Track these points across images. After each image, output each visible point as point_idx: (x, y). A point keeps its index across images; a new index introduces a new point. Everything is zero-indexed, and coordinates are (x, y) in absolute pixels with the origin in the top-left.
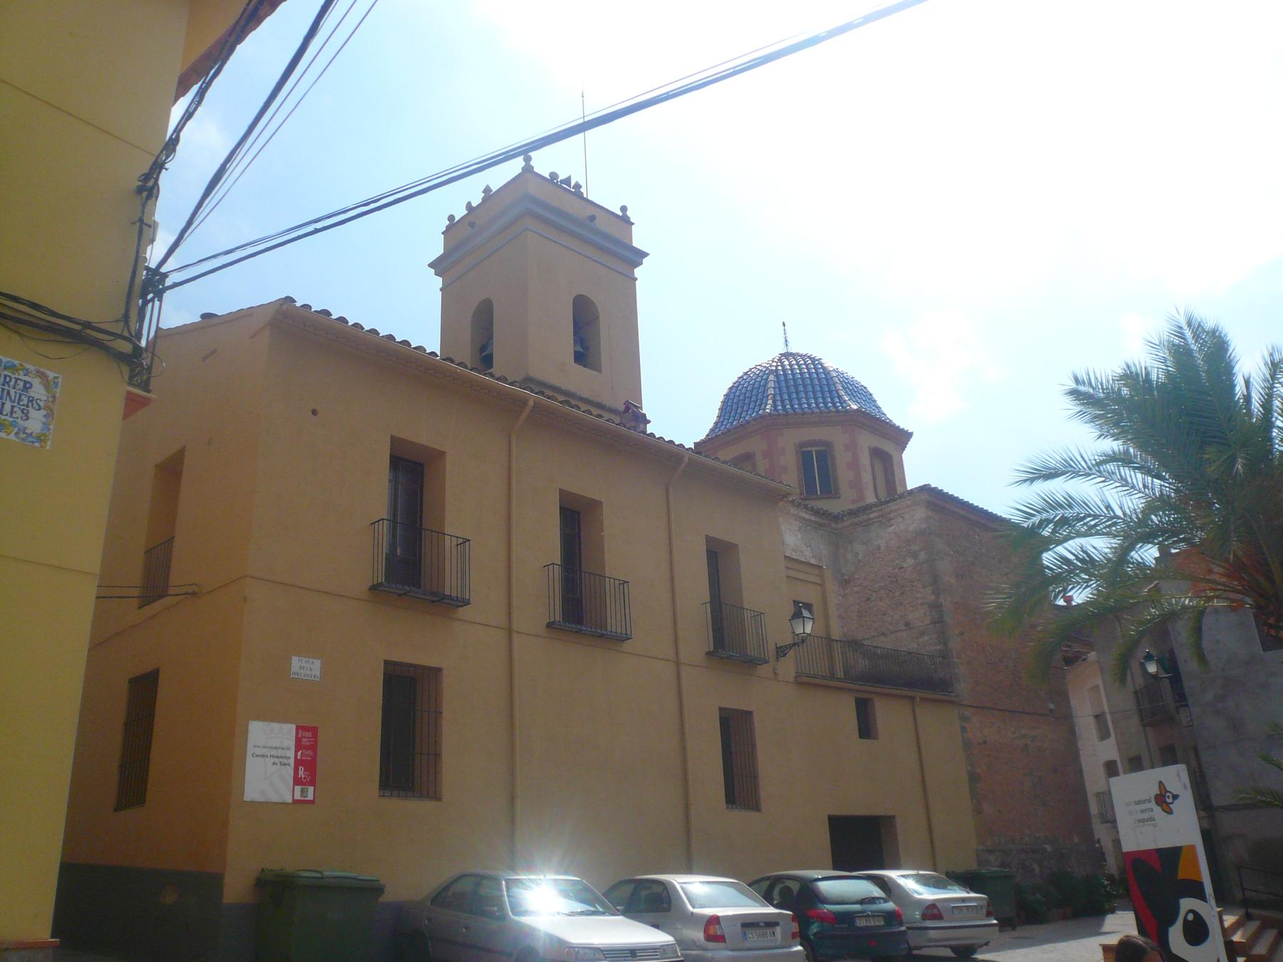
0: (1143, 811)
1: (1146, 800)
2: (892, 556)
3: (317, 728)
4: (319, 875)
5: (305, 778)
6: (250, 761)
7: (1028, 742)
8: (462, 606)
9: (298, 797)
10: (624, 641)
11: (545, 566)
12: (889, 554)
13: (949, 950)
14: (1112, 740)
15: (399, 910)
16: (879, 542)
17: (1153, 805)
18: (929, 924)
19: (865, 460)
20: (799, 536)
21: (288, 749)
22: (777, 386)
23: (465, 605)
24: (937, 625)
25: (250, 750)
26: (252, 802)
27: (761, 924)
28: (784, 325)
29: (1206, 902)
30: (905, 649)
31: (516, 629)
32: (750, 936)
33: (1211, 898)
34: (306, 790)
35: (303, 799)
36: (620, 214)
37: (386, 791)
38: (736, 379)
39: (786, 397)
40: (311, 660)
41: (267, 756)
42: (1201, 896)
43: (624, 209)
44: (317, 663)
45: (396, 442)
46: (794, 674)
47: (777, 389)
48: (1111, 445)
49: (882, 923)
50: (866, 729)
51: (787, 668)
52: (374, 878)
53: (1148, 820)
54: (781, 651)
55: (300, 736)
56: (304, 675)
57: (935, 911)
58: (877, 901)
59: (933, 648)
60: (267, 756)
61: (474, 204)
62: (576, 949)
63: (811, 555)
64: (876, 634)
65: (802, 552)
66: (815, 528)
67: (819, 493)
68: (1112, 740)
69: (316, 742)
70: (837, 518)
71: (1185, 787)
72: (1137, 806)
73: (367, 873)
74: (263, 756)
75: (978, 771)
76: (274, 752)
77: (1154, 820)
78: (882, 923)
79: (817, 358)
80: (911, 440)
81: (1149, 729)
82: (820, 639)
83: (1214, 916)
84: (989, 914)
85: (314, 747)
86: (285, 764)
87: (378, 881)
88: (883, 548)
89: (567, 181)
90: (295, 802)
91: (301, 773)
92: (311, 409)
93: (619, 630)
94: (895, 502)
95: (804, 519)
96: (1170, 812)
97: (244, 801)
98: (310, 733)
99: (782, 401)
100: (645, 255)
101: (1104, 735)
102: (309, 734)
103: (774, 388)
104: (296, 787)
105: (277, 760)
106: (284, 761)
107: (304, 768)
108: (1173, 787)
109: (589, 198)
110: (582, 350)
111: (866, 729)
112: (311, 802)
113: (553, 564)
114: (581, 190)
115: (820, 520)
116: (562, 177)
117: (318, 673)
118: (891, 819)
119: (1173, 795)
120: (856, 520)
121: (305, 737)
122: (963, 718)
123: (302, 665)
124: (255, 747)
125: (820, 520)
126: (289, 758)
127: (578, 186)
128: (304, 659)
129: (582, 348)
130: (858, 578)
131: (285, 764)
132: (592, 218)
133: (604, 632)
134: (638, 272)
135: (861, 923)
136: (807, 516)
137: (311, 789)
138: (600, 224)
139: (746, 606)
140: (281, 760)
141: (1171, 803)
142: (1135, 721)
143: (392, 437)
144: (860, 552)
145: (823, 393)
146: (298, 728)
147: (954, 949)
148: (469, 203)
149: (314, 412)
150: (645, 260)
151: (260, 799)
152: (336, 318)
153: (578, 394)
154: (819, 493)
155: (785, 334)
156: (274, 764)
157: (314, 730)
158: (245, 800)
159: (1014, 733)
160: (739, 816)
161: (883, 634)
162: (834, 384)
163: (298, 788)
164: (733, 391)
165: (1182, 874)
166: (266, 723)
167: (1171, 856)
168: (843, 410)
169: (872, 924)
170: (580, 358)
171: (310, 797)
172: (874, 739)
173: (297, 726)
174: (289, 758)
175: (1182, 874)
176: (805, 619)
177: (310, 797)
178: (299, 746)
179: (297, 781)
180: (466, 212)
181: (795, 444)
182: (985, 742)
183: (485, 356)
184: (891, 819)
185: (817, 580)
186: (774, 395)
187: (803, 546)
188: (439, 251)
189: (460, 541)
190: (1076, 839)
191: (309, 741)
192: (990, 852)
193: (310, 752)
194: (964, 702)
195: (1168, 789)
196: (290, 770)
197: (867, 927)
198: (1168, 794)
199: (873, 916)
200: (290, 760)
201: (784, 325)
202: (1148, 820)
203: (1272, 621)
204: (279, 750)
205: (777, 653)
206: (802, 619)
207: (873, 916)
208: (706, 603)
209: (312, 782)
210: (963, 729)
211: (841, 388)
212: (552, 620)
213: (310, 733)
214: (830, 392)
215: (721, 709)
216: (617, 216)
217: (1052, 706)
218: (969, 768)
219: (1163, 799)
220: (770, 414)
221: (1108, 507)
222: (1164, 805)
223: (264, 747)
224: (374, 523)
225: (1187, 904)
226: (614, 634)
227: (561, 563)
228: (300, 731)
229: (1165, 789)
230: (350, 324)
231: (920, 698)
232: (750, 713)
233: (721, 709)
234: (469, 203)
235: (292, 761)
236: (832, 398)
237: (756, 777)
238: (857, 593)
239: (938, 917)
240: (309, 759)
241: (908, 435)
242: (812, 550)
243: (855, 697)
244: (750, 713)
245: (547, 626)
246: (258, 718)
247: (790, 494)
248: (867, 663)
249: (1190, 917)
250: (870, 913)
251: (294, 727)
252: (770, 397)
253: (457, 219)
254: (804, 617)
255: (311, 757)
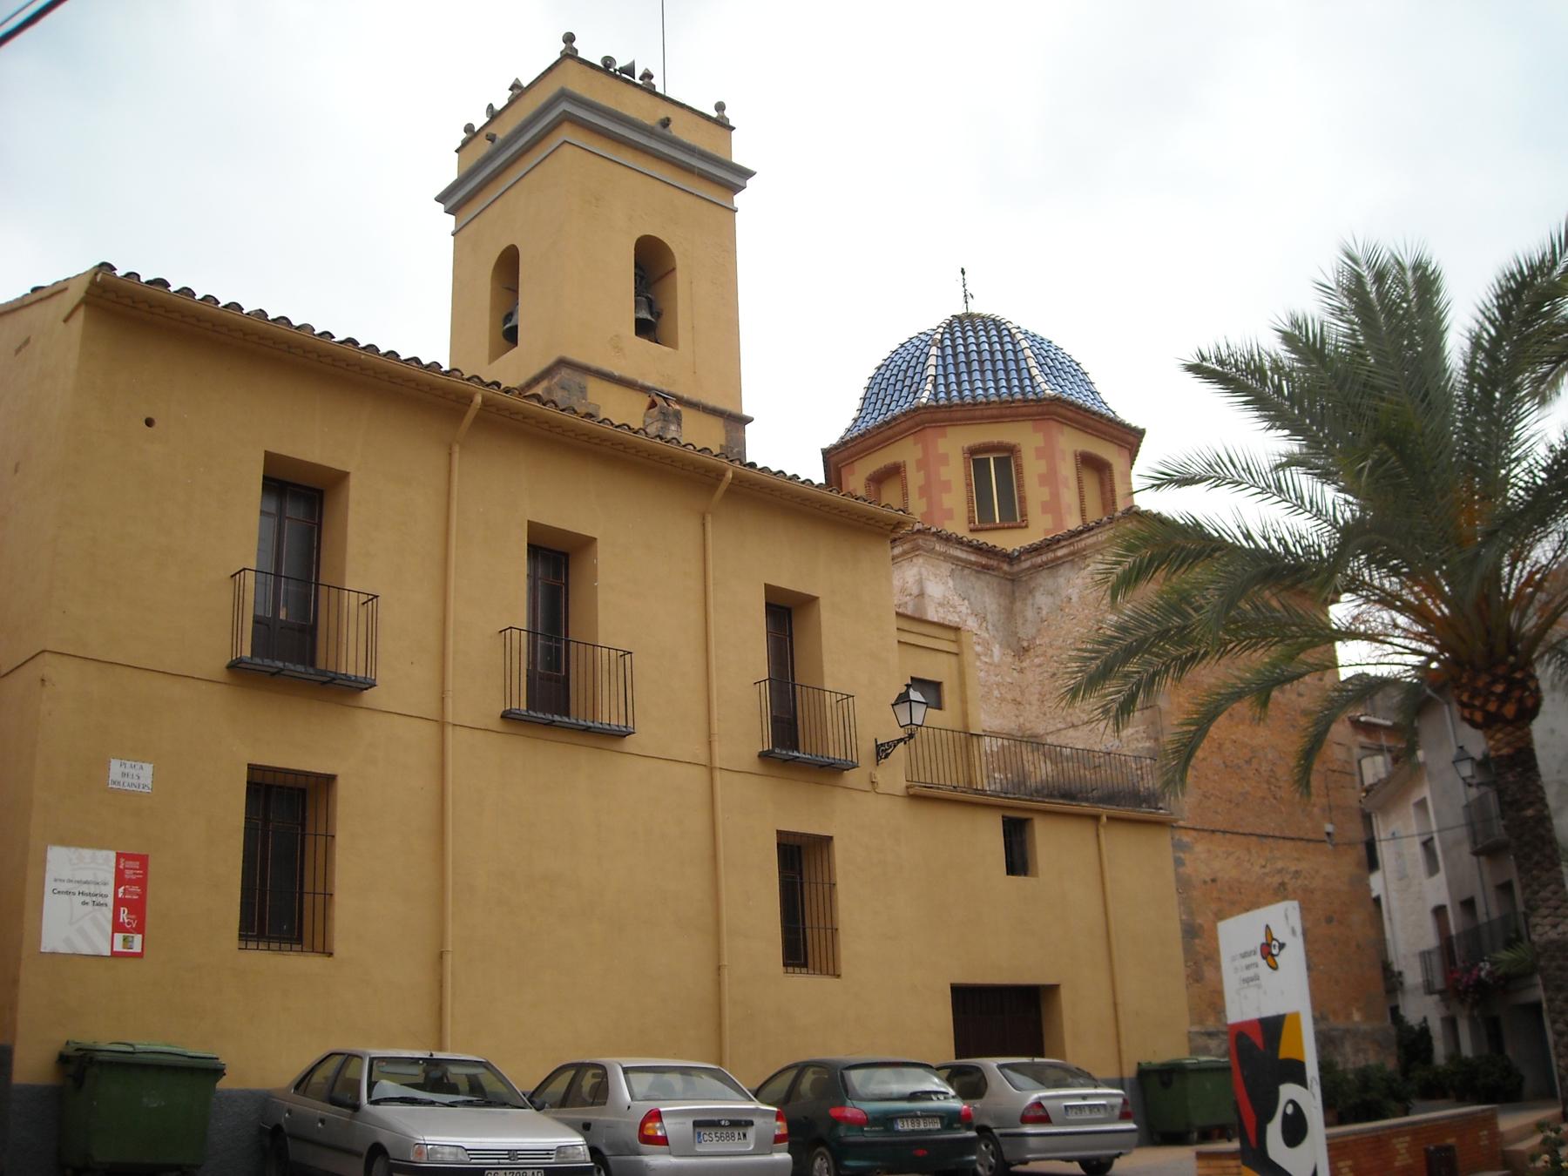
0: (1248, 967)
1: (1251, 952)
2: (1086, 611)
3: (147, 856)
4: (131, 1049)
5: (129, 923)
6: (50, 902)
7: (1286, 880)
8: (366, 689)
9: (118, 947)
10: (625, 736)
11: (501, 632)
12: (1083, 609)
13: (1076, 1164)
14: (1441, 877)
15: (264, 1101)
16: (1070, 591)
17: (1258, 958)
18: (1029, 1129)
19: (1067, 469)
20: (951, 583)
21: (105, 884)
22: (940, 362)
23: (371, 687)
24: (1145, 711)
25: (49, 885)
26: (53, 954)
27: (723, 1123)
28: (963, 272)
29: (1306, 1087)
30: (1103, 748)
31: (450, 721)
32: (706, 1137)
33: (1314, 1083)
34: (130, 939)
35: (126, 950)
36: (714, 114)
37: (260, 943)
38: (888, 354)
39: (952, 378)
40: (138, 764)
41: (74, 894)
42: (1301, 1080)
43: (720, 107)
44: (148, 769)
45: (271, 459)
46: (904, 784)
47: (940, 368)
48: (1294, 447)
49: (938, 1126)
50: (1018, 861)
51: (894, 774)
52: (215, 1056)
53: (1252, 979)
54: (882, 751)
55: (121, 867)
56: (129, 785)
57: (1041, 1113)
58: (934, 1097)
59: (1140, 746)
60: (74, 894)
61: (498, 107)
62: (429, 1147)
63: (969, 611)
64: (1063, 726)
65: (954, 607)
66: (977, 572)
67: (998, 521)
68: (1441, 877)
69: (145, 874)
70: (1009, 558)
71: (1294, 932)
72: (1243, 960)
73: (192, 1046)
74: (68, 893)
75: (1199, 921)
76: (85, 888)
77: (1258, 979)
78: (938, 1126)
79: (1003, 321)
80: (1144, 440)
81: (1483, 859)
82: (950, 733)
83: (1316, 1108)
84: (1125, 1116)
85: (142, 882)
86: (99, 904)
87: (217, 1059)
88: (1075, 599)
89: (630, 70)
90: (115, 955)
91: (124, 916)
92: (144, 419)
93: (614, 722)
94: (1092, 533)
95: (958, 559)
96: (1274, 967)
97: (41, 953)
98: (138, 863)
99: (947, 386)
100: (747, 174)
101: (1433, 868)
102: (136, 864)
103: (936, 367)
104: (116, 934)
105: (88, 899)
106: (101, 900)
107: (128, 910)
108: (1280, 934)
109: (667, 95)
110: (649, 317)
111: (1018, 861)
112: (139, 955)
113: (511, 628)
114: (653, 81)
115: (984, 561)
116: (621, 63)
117: (149, 782)
118: (951, 984)
119: (1279, 943)
120: (1039, 560)
121: (127, 869)
122: (1178, 846)
123: (126, 771)
124: (56, 880)
125: (984, 561)
126: (106, 896)
127: (647, 76)
128: (128, 763)
129: (652, 314)
130: (1040, 645)
131: (99, 904)
132: (666, 123)
133: (591, 724)
134: (739, 200)
135: (903, 1126)
136: (963, 555)
137: (138, 938)
138: (681, 129)
139: (828, 685)
140: (94, 899)
141: (1277, 955)
142: (1466, 848)
143: (267, 454)
144: (1043, 606)
145: (1007, 372)
146: (119, 856)
147: (1084, 1163)
148: (491, 106)
149: (149, 423)
150: (749, 182)
151: (62, 949)
152: (177, 289)
153: (640, 381)
154: (998, 521)
155: (964, 286)
156: (84, 903)
157: (143, 860)
158: (42, 950)
159: (1264, 867)
160: (803, 983)
161: (1073, 726)
162: (1025, 360)
163: (119, 937)
164: (882, 371)
165: (1285, 1052)
166: (73, 849)
167: (1273, 1027)
168: (1034, 397)
169: (922, 1127)
170: (645, 328)
171: (137, 948)
172: (1033, 876)
173: (117, 853)
174: (106, 896)
175: (1285, 1052)
176: (913, 704)
177: (137, 948)
178: (120, 879)
179: (118, 927)
180: (487, 119)
181: (963, 447)
182: (1213, 881)
183: (510, 328)
184: (951, 984)
185: (952, 648)
186: (936, 377)
187: (955, 597)
188: (451, 176)
189: (364, 598)
190: (1357, 1017)
191: (134, 874)
192: (1210, 1035)
193: (136, 889)
194: (1181, 823)
195: (1275, 936)
196: (108, 913)
197: (913, 1131)
198: (1274, 942)
199: (922, 1117)
200: (107, 899)
201: (963, 272)
202: (1252, 979)
203: (1465, 698)
204: (87, 891)
205: (878, 754)
206: (908, 703)
207: (922, 1117)
208: (760, 682)
209: (140, 929)
210: (1179, 862)
211: (1035, 365)
212: (508, 708)
213: (138, 863)
214: (1019, 371)
215: (779, 832)
216: (708, 118)
217: (1329, 828)
218: (1184, 917)
219: (1269, 951)
220: (926, 407)
221: (1248, 536)
222: (1269, 957)
223: (70, 881)
224: (235, 575)
225: (1288, 1091)
226: (608, 727)
227: (529, 626)
228: (122, 860)
229: (1272, 936)
230: (197, 297)
231: (1108, 818)
232: (830, 838)
233: (779, 832)
234: (491, 106)
235: (110, 901)
236: (1021, 380)
237: (835, 930)
238: (1040, 666)
239: (1045, 1119)
240: (137, 897)
241: (1139, 434)
242: (970, 603)
243: (1003, 817)
244: (830, 838)
245: (502, 717)
246: (64, 842)
247: (904, 523)
248: (1049, 769)
249: (1290, 1110)
250: (919, 1113)
251: (113, 855)
252: (930, 378)
253: (476, 129)
254: (911, 701)
255: (138, 895)
